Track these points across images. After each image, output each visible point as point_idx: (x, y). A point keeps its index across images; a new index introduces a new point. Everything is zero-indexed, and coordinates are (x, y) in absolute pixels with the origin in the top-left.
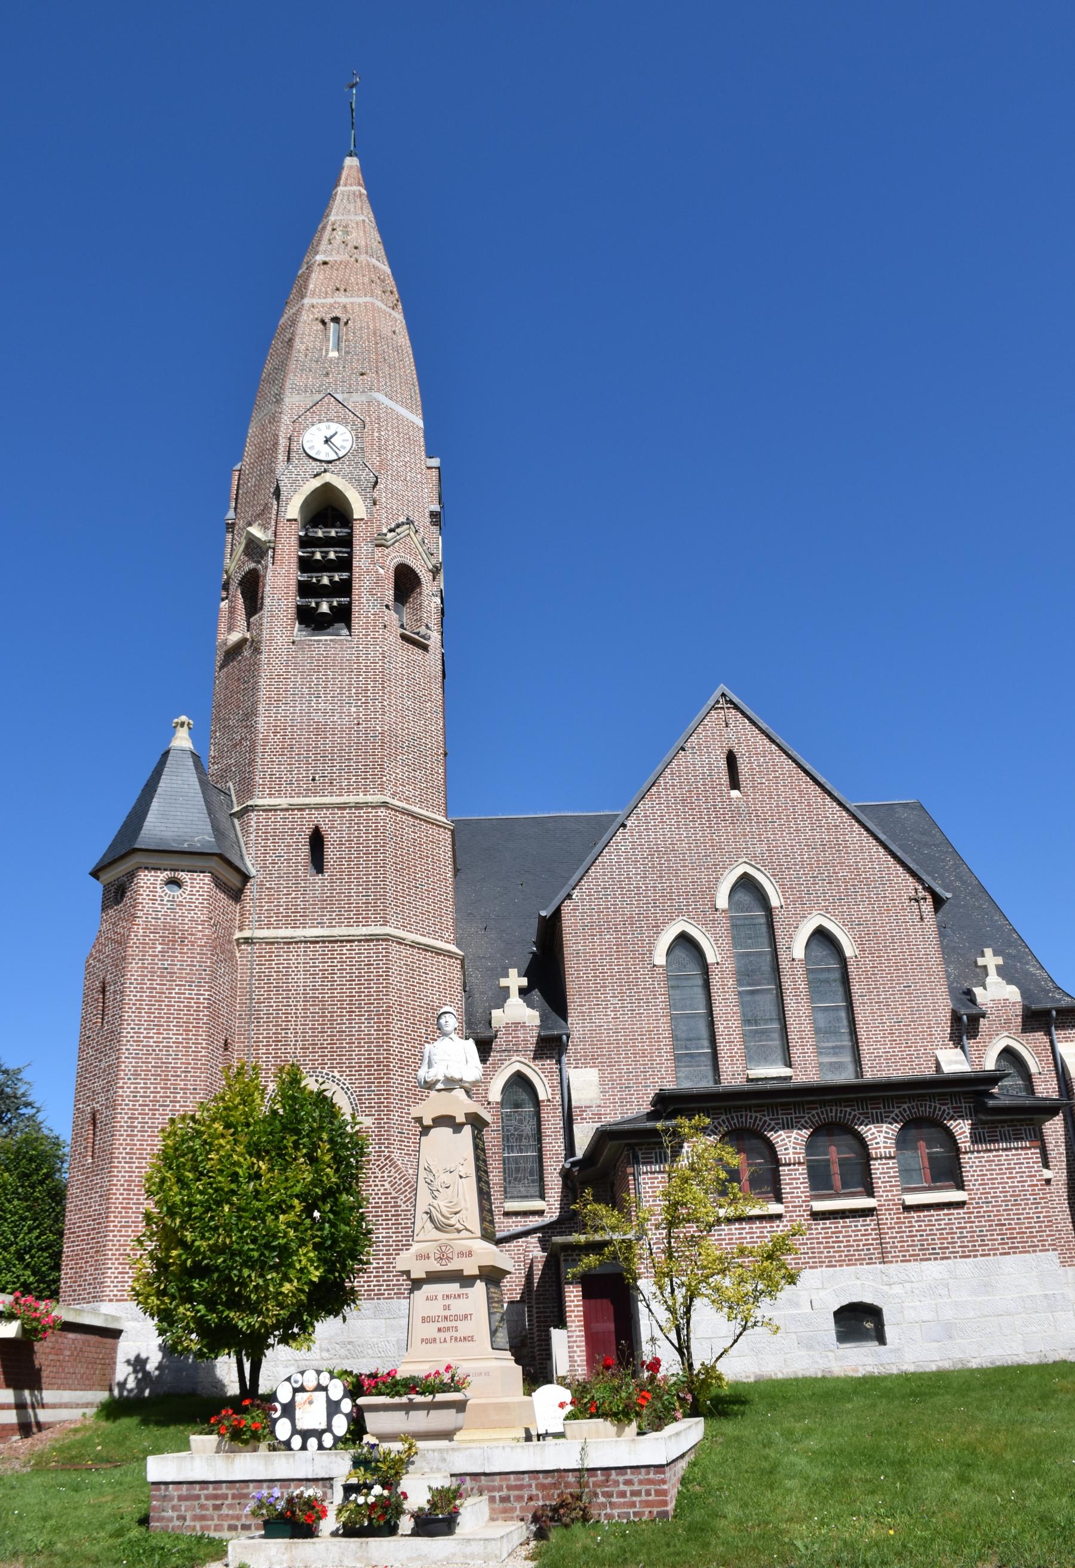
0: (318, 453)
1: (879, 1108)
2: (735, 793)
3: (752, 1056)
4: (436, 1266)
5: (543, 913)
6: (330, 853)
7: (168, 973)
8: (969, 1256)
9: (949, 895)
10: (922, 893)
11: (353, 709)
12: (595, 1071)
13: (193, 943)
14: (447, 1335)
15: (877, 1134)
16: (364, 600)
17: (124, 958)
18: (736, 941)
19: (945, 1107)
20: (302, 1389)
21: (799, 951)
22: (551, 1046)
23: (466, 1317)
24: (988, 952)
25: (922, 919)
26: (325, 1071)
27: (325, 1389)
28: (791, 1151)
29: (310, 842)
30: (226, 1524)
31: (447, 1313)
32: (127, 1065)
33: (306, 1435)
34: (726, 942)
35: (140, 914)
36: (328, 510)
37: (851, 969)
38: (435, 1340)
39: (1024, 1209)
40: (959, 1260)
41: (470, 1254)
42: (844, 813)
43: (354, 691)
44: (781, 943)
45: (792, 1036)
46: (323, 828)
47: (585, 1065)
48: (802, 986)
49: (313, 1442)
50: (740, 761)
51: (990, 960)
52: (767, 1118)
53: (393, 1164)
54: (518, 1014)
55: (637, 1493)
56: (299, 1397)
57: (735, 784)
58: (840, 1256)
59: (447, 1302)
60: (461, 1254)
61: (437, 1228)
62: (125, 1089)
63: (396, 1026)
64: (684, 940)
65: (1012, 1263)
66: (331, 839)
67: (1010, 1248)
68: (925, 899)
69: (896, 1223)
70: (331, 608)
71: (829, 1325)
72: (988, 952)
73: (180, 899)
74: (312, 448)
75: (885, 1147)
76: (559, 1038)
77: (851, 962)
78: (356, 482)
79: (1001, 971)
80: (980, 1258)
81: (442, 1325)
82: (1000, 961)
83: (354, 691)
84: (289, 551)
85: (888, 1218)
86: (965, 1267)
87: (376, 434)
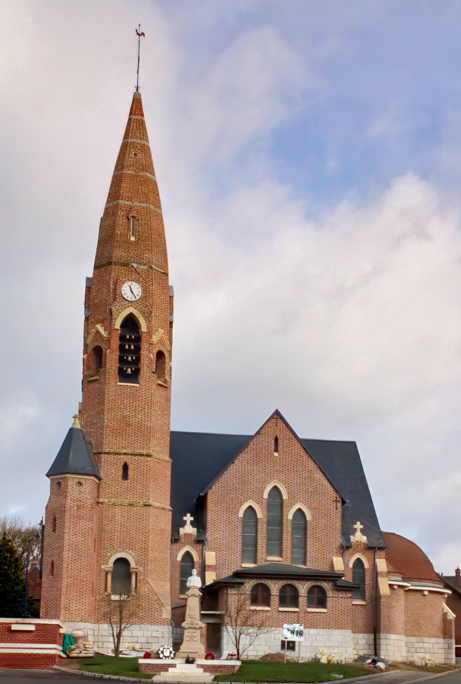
0: (125, 294)
2: (276, 454)
3: (269, 553)
4: (190, 626)
5: (201, 494)
6: (130, 473)
11: (140, 416)
13: (87, 507)
16: (145, 370)
17: (64, 511)
18: (269, 511)
21: (290, 517)
22: (200, 541)
24: (358, 523)
25: (337, 509)
32: (66, 548)
33: (166, 657)
34: (265, 511)
35: (68, 495)
36: (131, 323)
37: (308, 525)
44: (285, 513)
48: (290, 529)
50: (279, 441)
53: (148, 583)
54: (189, 529)
62: (66, 555)
63: (151, 536)
65: (336, 632)
66: (131, 467)
68: (339, 501)
70: (132, 371)
72: (358, 523)
74: (125, 294)
76: (203, 541)
77: (308, 522)
78: (143, 312)
84: (116, 343)
85: (301, 615)
86: (323, 631)
87: (151, 288)
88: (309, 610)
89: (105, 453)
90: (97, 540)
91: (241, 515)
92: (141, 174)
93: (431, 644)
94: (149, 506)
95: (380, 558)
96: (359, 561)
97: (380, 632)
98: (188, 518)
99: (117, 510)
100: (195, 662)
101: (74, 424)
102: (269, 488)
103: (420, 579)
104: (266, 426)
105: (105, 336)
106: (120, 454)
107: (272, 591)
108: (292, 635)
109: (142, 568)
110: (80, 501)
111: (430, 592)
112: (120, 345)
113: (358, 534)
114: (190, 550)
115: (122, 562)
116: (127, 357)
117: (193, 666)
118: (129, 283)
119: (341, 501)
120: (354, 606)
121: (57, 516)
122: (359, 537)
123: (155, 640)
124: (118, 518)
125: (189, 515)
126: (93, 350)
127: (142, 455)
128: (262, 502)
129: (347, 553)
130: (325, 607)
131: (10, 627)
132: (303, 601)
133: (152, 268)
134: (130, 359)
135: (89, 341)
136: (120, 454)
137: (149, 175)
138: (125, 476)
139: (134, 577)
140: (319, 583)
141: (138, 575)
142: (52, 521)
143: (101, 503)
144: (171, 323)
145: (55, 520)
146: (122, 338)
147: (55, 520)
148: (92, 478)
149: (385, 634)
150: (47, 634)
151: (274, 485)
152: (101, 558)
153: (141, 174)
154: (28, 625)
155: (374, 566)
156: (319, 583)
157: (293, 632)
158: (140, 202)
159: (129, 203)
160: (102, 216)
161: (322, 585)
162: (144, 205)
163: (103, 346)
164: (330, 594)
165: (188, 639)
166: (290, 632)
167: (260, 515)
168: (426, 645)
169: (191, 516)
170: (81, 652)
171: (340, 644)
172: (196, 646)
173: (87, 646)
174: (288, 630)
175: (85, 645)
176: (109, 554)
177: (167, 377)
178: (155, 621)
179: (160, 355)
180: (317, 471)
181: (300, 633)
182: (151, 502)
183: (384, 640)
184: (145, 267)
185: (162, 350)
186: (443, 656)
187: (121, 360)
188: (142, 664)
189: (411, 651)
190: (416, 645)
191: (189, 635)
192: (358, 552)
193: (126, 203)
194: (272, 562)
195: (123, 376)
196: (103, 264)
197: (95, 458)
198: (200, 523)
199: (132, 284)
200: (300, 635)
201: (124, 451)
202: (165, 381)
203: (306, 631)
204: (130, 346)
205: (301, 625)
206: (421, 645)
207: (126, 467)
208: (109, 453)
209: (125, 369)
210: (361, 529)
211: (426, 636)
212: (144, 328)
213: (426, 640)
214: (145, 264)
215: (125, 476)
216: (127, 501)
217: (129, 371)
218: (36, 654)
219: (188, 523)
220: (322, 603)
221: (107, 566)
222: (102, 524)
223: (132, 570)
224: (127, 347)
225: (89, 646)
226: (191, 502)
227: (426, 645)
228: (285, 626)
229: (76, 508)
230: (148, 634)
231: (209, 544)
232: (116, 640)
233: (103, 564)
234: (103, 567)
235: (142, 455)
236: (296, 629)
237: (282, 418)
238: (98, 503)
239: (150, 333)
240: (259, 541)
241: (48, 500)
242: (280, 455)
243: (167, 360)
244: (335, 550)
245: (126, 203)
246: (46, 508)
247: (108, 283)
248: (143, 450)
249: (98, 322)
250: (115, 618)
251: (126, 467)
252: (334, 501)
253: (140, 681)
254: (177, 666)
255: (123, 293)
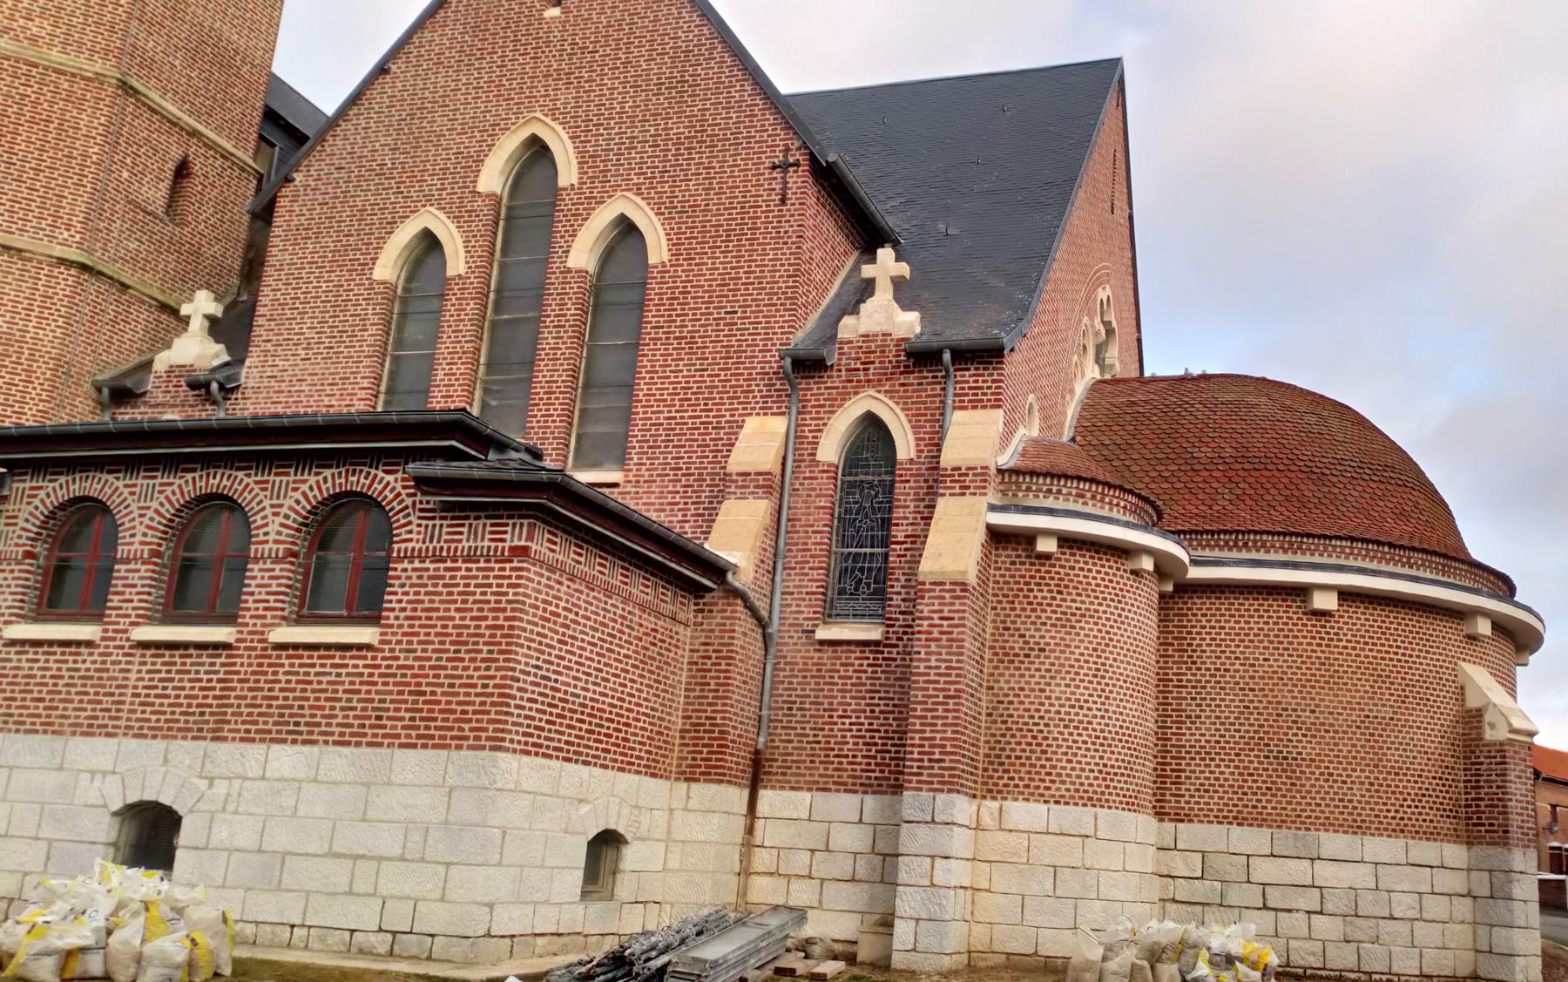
1: (288, 474)
8: (348, 743)
15: (271, 518)
19: (390, 478)
25: (783, 202)
28: (139, 538)
39: (466, 668)
40: (331, 748)
52: (250, 480)
58: (158, 721)
65: (412, 764)
67: (419, 737)
68: (797, 164)
69: (254, 673)
71: (105, 829)
75: (276, 542)
80: (365, 750)
86: (338, 761)
96: (872, 423)
103: (1296, 536)
107: (124, 536)
111: (1347, 595)
113: (884, 295)
120: (829, 652)
129: (814, 390)
151: (524, 133)
167: (457, 261)
183: (922, 831)
186: (1460, 935)
189: (1233, 899)
190: (1264, 870)
206: (1298, 871)
211: (1329, 825)
213: (1334, 843)
242: (566, 11)
244: (759, 387)
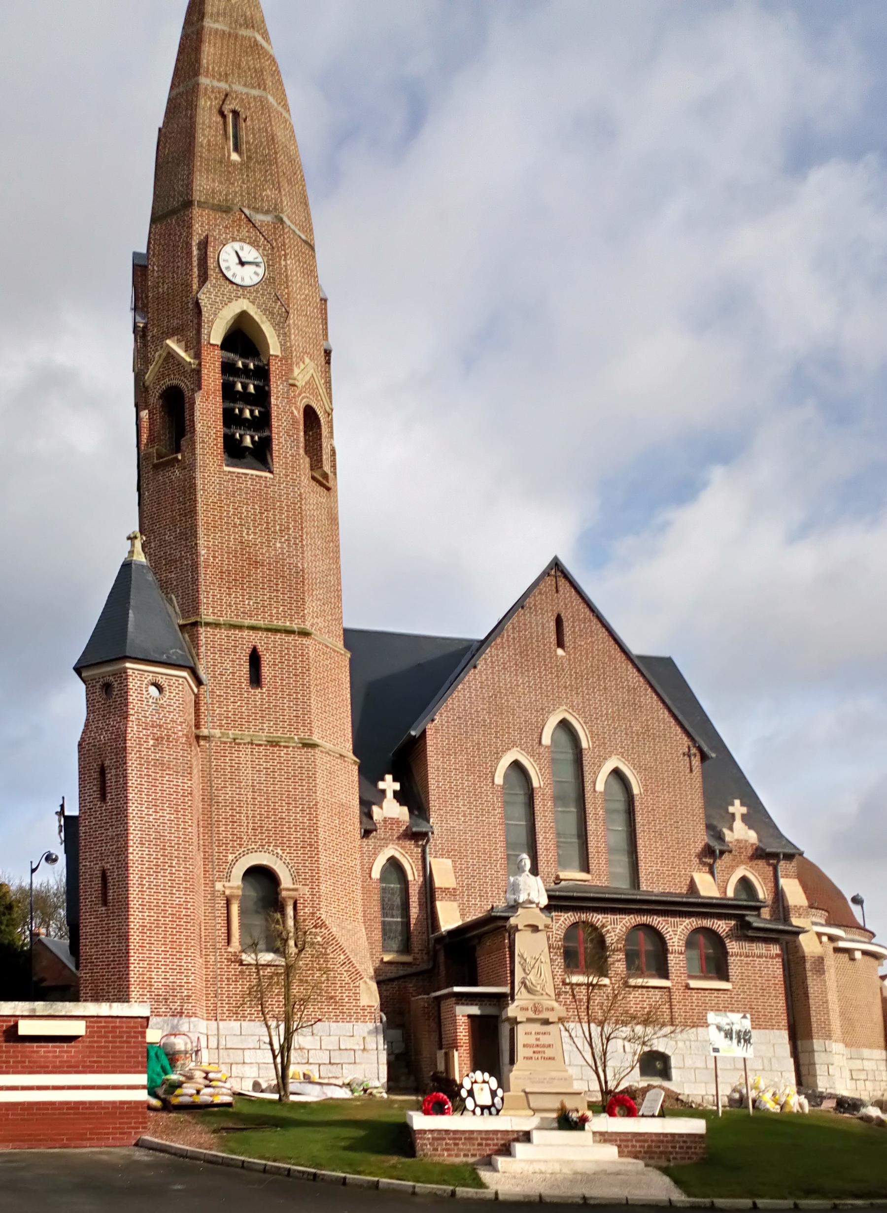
0: (228, 268)
2: (560, 652)
4: (531, 1015)
5: (413, 733)
6: (266, 671)
7: (161, 765)
9: (714, 755)
10: (694, 750)
11: (278, 545)
12: (449, 861)
14: (540, 1056)
20: (476, 1082)
21: (600, 787)
22: (416, 836)
23: (549, 1046)
24: (737, 802)
25: (691, 771)
26: (271, 848)
27: (487, 1082)
29: (250, 659)
30: (462, 1154)
31: (538, 1043)
33: (483, 1108)
36: (242, 339)
37: (637, 803)
38: (531, 1058)
41: (553, 1009)
42: (641, 679)
43: (278, 527)
45: (592, 850)
46: (260, 649)
47: (442, 856)
49: (486, 1111)
50: (565, 624)
51: (737, 808)
54: (391, 810)
55: (690, 1148)
56: (475, 1085)
57: (560, 644)
59: (538, 1036)
60: (547, 1009)
61: (529, 992)
62: (135, 853)
63: (321, 818)
64: (516, 765)
66: (266, 659)
72: (737, 802)
73: (162, 702)
74: (228, 268)
77: (637, 798)
78: (269, 312)
79: (745, 818)
81: (535, 1049)
82: (744, 810)
83: (278, 527)
84: (212, 377)
87: (283, 263)
88: (693, 984)
89: (207, 624)
90: (201, 823)
91: (499, 780)
92: (243, 32)
93: (874, 1062)
94: (314, 746)
95: (787, 876)
97: (809, 1036)
98: (389, 785)
99: (244, 755)
100: (587, 1126)
101: (131, 552)
102: (552, 722)
104: (536, 591)
105: (188, 359)
106: (240, 627)
108: (727, 1041)
109: (307, 889)
110: (161, 726)
111: (865, 953)
112: (223, 384)
113: (738, 824)
114: (398, 855)
115: (262, 876)
116: (241, 411)
117: (582, 1138)
118: (237, 245)
119: (698, 755)
121: (107, 763)
122: (741, 833)
123: (348, 1057)
124: (247, 775)
125: (389, 778)
126: (161, 396)
127: (289, 632)
128: (539, 754)
130: (725, 977)
131: (16, 1026)
132: (676, 961)
133: (281, 221)
134: (247, 414)
135: (149, 376)
136: (240, 627)
137: (259, 38)
138: (256, 679)
139: (290, 911)
140: (707, 923)
141: (300, 906)
142: (96, 775)
143: (205, 738)
144: (328, 353)
145: (102, 771)
146: (228, 368)
147: (102, 771)
148: (184, 674)
149: (821, 1041)
150: (117, 1045)
151: (560, 718)
152: (215, 866)
153: (243, 32)
154: (66, 1019)
155: (779, 895)
156: (707, 923)
157: (729, 1034)
158: (245, 85)
159: (223, 85)
160: (161, 125)
161: (715, 927)
162: (255, 92)
163: (185, 384)
164: (733, 947)
165: (529, 1052)
166: (723, 1034)
168: (868, 1065)
169: (395, 780)
170: (198, 1092)
171: (766, 1062)
172: (554, 1074)
173: (211, 1076)
174: (719, 1028)
175: (207, 1073)
176: (230, 857)
177: (327, 468)
178: (343, 1012)
179: (310, 415)
180: (646, 690)
181: (744, 1038)
182: (316, 739)
184: (268, 218)
185: (314, 406)
187: (230, 419)
188: (424, 1132)
191: (531, 1040)
192: (742, 862)
193: (216, 83)
194: (571, 883)
195: (233, 451)
196: (172, 206)
197: (184, 638)
198: (413, 797)
199: (242, 249)
200: (745, 1041)
201: (247, 622)
202: (325, 476)
203: (755, 1035)
204: (245, 387)
205: (744, 1017)
207: (255, 659)
208: (217, 625)
209: (238, 436)
210: (743, 816)
212: (274, 348)
214: (267, 212)
215: (256, 679)
216: (263, 736)
217: (248, 441)
218: (97, 1103)
219: (390, 794)
220: (718, 967)
221: (227, 884)
222: (211, 786)
223: (284, 894)
224: (239, 387)
225: (219, 1076)
226: (391, 751)
227: (868, 1065)
228: (712, 1017)
229: (151, 742)
230: (330, 1043)
231: (435, 842)
232: (279, 1060)
233: (220, 879)
234: (219, 886)
235: (289, 632)
236: (736, 1028)
237: (566, 576)
238: (198, 737)
239: (287, 359)
240: (540, 838)
241: (82, 727)
243: (325, 431)
245: (216, 83)
246: (80, 745)
247: (188, 245)
248: (291, 621)
249: (169, 335)
250: (275, 1003)
251: (255, 659)
252: (684, 754)
253: (453, 1193)
254: (536, 1136)
255: (223, 265)
